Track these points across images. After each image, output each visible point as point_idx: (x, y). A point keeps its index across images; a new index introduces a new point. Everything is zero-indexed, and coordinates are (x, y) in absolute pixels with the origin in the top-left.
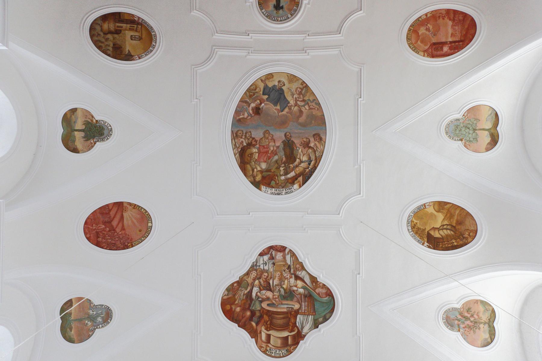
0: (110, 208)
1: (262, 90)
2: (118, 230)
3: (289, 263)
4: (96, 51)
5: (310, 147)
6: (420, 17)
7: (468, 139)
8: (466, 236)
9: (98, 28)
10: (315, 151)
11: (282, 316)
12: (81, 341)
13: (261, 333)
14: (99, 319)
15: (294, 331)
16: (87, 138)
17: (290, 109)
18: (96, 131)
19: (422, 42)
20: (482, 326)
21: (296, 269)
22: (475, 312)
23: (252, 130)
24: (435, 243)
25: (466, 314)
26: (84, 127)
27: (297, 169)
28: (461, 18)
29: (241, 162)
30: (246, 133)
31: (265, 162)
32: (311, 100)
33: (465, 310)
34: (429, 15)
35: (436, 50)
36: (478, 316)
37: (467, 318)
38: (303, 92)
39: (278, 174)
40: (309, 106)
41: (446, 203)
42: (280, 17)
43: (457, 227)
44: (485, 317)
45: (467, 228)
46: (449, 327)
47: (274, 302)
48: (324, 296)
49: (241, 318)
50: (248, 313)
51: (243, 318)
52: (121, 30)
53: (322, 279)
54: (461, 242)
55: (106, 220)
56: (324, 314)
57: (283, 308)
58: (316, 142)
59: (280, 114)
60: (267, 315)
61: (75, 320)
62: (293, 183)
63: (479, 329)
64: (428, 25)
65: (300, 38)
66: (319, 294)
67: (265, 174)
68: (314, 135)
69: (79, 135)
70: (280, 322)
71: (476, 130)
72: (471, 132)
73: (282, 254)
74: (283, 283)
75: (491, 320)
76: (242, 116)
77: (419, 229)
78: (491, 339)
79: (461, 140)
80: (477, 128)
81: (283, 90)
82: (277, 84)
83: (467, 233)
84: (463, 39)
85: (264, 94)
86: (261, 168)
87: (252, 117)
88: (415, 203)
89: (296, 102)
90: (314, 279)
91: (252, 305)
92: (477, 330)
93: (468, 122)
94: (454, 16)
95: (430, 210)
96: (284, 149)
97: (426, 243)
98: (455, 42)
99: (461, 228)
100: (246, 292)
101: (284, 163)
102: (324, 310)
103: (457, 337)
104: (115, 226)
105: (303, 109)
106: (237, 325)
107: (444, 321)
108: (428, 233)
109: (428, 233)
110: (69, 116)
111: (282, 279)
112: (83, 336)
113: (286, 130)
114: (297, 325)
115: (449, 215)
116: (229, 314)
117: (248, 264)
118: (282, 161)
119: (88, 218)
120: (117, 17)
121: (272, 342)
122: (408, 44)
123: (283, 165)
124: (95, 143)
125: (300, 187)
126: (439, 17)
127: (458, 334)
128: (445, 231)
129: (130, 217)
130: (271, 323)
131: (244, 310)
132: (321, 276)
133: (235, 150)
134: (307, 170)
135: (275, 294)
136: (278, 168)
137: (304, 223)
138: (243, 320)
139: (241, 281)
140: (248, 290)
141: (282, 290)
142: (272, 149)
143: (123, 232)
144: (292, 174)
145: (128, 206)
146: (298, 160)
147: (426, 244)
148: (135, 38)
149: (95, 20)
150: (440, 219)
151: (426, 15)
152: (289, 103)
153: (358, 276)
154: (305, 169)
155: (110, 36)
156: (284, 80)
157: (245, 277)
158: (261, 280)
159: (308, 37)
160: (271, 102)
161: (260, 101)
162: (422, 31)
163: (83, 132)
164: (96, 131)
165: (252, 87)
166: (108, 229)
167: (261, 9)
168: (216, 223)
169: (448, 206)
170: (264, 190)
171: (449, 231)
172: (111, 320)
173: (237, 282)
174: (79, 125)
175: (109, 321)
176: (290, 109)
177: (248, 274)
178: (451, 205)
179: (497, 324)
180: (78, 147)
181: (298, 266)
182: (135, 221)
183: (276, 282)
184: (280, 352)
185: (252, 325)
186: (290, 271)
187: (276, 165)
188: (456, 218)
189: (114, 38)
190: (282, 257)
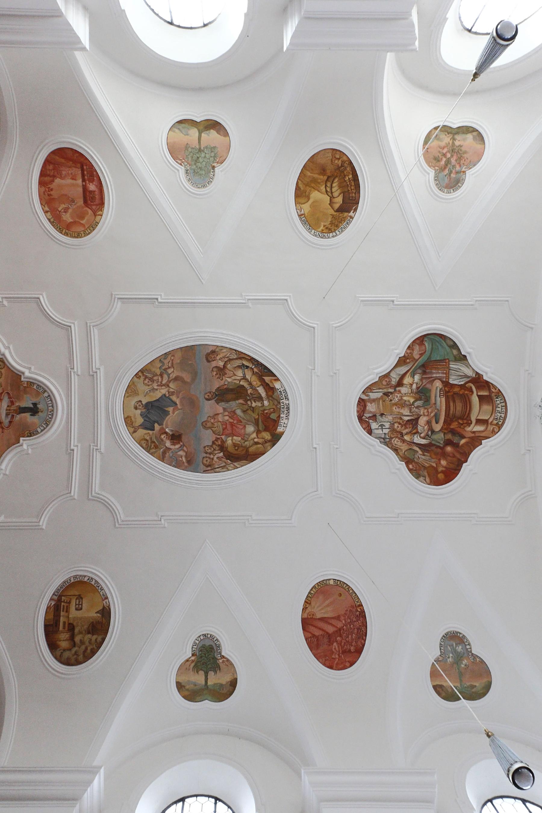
0: (310, 635)
1: (149, 431)
2: (339, 625)
3: (381, 394)
4: (99, 657)
5: (224, 366)
6: (49, 220)
7: (212, 159)
8: (340, 163)
9: (67, 654)
10: (230, 360)
11: (452, 404)
12: (488, 673)
13: (474, 432)
14: (459, 648)
15: (471, 387)
16: (216, 668)
17: (173, 393)
18: (207, 657)
19: (82, 218)
20: (457, 143)
21: (389, 384)
22: (439, 152)
23: (203, 446)
24: (350, 202)
25: (443, 163)
26: (202, 673)
27: (254, 383)
28: (51, 167)
29: (246, 460)
30: (206, 453)
31: (245, 427)
32: (161, 364)
33: (438, 164)
34: (47, 209)
35: (93, 199)
36: (443, 148)
37: (448, 162)
38: (149, 375)
39: (262, 409)
40: (169, 368)
41: (297, 188)
42: (48, 407)
43: (329, 174)
44: (446, 139)
45: (330, 162)
46: (459, 184)
47: (432, 415)
48: (424, 348)
49: (455, 459)
50: (449, 449)
51: (454, 456)
52: (69, 624)
53: (401, 351)
54: (348, 169)
55: (326, 640)
56: (447, 348)
57: (441, 402)
58: (218, 358)
59: (179, 406)
60: (450, 424)
61: (461, 681)
62: (273, 389)
63: (460, 146)
64: (60, 209)
65: (76, 381)
66: (421, 355)
67: (261, 427)
68: (208, 361)
69: (214, 679)
70: (459, 406)
71: (200, 148)
72: (203, 155)
73: (369, 404)
74: (407, 403)
75: (449, 131)
76: (184, 458)
77: (332, 223)
78: (473, 131)
79: (213, 167)
80: (198, 147)
81: (147, 404)
82: (139, 412)
83: (336, 162)
84: (79, 165)
85: (153, 430)
86: (253, 432)
87: (184, 445)
88: (296, 225)
89: (164, 385)
90: (402, 361)
91: (439, 444)
92: (462, 148)
93: (190, 159)
94: (49, 175)
95: (306, 208)
96: (227, 401)
97: (350, 215)
98: (83, 175)
99: (330, 168)
100: (420, 452)
101: (246, 401)
102: (442, 347)
103: (472, 174)
104: (335, 629)
105: (173, 376)
106: (464, 465)
107: (452, 191)
108: (337, 211)
109: (337, 211)
110: (187, 693)
111: (402, 404)
112: (481, 670)
113: (202, 399)
114: (462, 383)
115: (312, 184)
116: (450, 474)
117: (382, 449)
118: (243, 404)
119: (324, 665)
120: (51, 630)
121: (486, 418)
122: (85, 236)
123: (249, 403)
124: (223, 657)
125: (278, 380)
126: (49, 195)
127: (469, 173)
128: (334, 190)
129: (322, 609)
130: (462, 418)
131: (444, 455)
132: (397, 351)
133: (230, 468)
134: (255, 370)
135: (422, 413)
136: (253, 409)
137: (325, 380)
138: (458, 456)
139: (405, 459)
140: (417, 449)
141: (416, 404)
142: (227, 418)
143: (342, 618)
144: (261, 391)
145: (307, 611)
146: (242, 383)
147: (351, 214)
148: (79, 605)
149: (56, 658)
150: (318, 196)
151: (46, 212)
152: (165, 395)
153: (396, 303)
154: (254, 373)
155: (77, 639)
156: (134, 401)
157: (401, 453)
158: (404, 432)
159: (75, 370)
160: (164, 419)
161: (163, 434)
162: (67, 218)
163: (208, 672)
164: (207, 657)
165: (144, 445)
166: (339, 638)
167: (38, 433)
168: (327, 492)
169: (300, 185)
170: (283, 428)
171: (334, 185)
172: (460, 633)
173: (407, 464)
174: (199, 678)
175: (461, 636)
176: (173, 393)
177: (396, 450)
178: (300, 182)
179: (454, 124)
180: (229, 680)
181: (384, 383)
182: (327, 602)
183: (406, 411)
184: (500, 406)
185: (464, 444)
186: (391, 393)
187: (250, 412)
188: (316, 176)
189: (80, 633)
190: (373, 404)
